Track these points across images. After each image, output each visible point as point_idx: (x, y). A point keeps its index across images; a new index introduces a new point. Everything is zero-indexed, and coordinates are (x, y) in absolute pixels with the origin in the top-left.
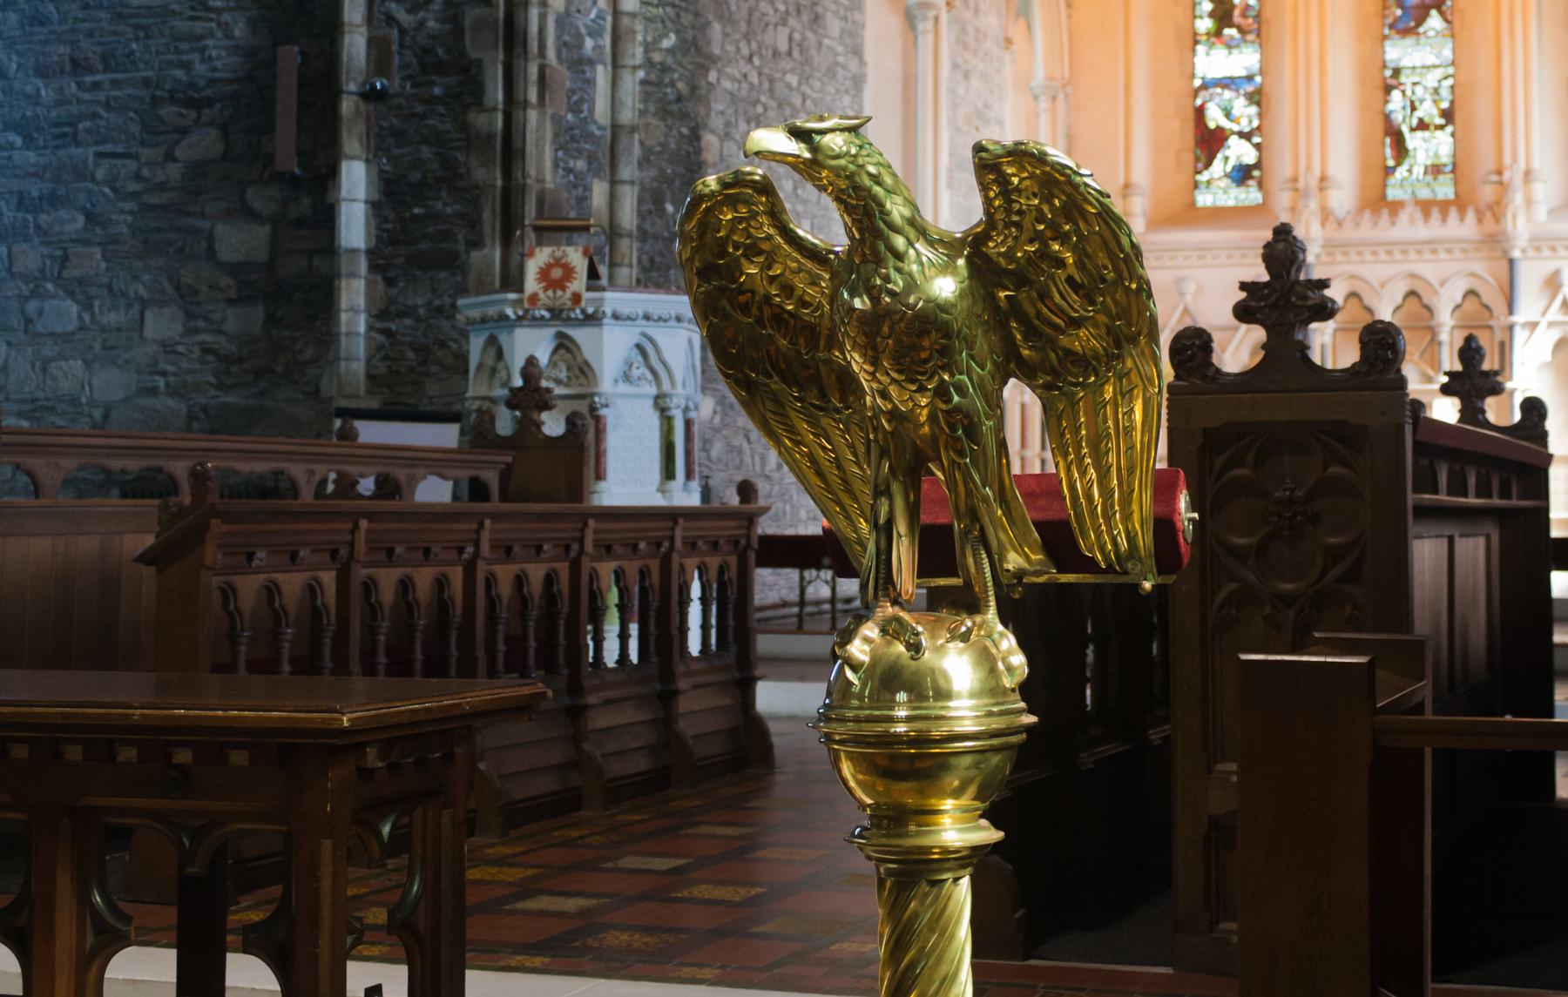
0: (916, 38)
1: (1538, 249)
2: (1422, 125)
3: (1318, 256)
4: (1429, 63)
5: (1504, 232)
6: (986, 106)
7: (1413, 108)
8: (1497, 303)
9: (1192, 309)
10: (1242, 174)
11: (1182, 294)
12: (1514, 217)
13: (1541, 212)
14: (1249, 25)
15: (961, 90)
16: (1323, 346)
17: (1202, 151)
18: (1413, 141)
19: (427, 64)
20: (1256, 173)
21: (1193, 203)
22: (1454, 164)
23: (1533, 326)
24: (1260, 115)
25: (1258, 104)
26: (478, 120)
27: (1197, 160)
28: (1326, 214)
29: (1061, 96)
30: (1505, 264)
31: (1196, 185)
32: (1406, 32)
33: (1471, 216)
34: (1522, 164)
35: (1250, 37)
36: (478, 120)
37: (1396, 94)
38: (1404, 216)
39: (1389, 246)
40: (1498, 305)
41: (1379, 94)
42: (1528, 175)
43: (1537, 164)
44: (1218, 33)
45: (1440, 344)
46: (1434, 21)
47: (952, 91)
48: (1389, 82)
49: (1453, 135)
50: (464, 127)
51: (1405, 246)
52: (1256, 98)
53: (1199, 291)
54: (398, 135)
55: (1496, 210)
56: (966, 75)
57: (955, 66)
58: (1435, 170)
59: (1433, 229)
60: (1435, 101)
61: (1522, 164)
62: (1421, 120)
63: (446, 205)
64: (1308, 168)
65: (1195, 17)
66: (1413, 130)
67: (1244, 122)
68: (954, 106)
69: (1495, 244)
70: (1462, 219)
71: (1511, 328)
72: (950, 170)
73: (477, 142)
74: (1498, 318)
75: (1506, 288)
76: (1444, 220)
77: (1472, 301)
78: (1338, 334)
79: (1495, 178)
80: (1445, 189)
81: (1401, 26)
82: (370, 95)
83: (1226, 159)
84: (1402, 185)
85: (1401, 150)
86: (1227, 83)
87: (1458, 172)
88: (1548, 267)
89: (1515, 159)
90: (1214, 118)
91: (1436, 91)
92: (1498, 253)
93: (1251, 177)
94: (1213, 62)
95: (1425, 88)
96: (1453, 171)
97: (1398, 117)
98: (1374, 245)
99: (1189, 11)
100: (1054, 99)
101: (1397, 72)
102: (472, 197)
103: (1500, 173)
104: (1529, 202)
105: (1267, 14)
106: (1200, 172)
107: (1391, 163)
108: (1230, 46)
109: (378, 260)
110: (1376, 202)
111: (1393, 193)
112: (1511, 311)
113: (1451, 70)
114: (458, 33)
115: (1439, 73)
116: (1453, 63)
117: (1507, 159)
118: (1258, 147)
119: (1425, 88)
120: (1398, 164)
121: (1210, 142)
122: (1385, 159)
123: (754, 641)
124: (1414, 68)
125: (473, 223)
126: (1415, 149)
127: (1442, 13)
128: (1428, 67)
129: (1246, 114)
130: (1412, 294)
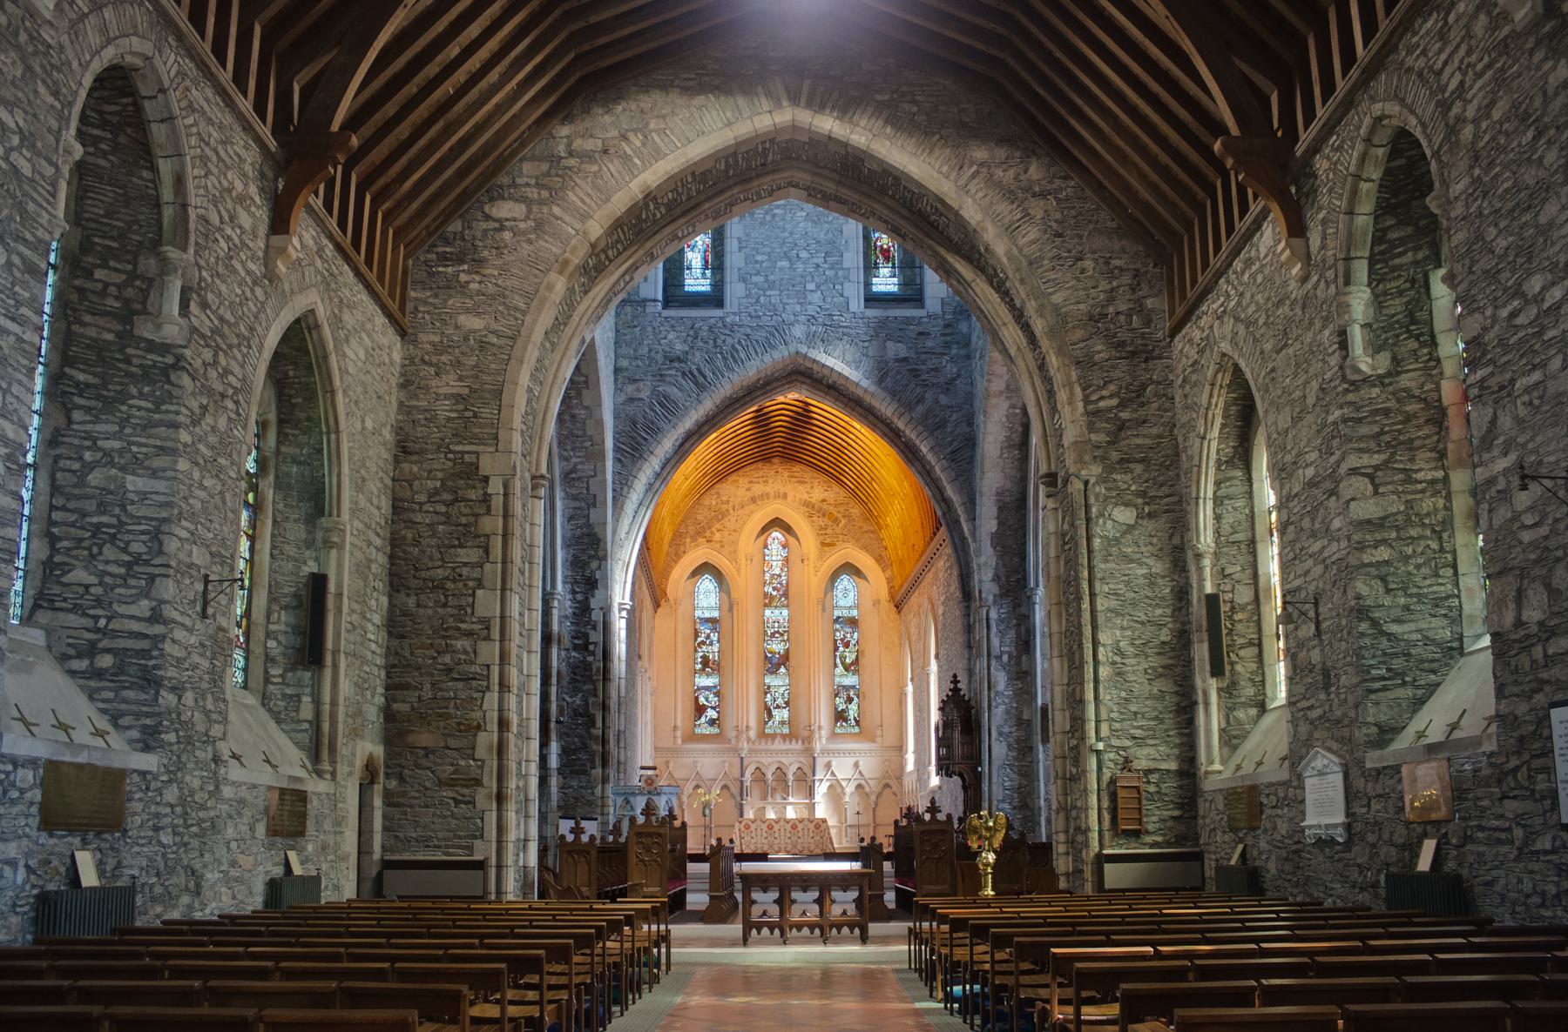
2: (778, 707)
8: (809, 773)
10: (712, 722)
18: (775, 712)
19: (576, 713)
26: (594, 731)
28: (749, 739)
32: (772, 673)
36: (594, 731)
38: (776, 741)
39: (771, 752)
40: (809, 773)
42: (820, 728)
44: (703, 670)
46: (783, 670)
48: (767, 690)
50: (589, 733)
51: (777, 752)
52: (717, 694)
54: (567, 734)
55: (808, 739)
58: (782, 723)
59: (787, 746)
63: (583, 756)
69: (809, 752)
73: (591, 737)
80: (786, 730)
82: (558, 722)
85: (770, 716)
86: (707, 688)
88: (827, 759)
90: (702, 700)
94: (703, 681)
101: (769, 687)
102: (592, 754)
104: (820, 737)
105: (723, 664)
108: (708, 675)
109: (560, 771)
110: (762, 735)
111: (767, 731)
114: (587, 705)
121: (700, 710)
125: (593, 762)
129: (714, 700)
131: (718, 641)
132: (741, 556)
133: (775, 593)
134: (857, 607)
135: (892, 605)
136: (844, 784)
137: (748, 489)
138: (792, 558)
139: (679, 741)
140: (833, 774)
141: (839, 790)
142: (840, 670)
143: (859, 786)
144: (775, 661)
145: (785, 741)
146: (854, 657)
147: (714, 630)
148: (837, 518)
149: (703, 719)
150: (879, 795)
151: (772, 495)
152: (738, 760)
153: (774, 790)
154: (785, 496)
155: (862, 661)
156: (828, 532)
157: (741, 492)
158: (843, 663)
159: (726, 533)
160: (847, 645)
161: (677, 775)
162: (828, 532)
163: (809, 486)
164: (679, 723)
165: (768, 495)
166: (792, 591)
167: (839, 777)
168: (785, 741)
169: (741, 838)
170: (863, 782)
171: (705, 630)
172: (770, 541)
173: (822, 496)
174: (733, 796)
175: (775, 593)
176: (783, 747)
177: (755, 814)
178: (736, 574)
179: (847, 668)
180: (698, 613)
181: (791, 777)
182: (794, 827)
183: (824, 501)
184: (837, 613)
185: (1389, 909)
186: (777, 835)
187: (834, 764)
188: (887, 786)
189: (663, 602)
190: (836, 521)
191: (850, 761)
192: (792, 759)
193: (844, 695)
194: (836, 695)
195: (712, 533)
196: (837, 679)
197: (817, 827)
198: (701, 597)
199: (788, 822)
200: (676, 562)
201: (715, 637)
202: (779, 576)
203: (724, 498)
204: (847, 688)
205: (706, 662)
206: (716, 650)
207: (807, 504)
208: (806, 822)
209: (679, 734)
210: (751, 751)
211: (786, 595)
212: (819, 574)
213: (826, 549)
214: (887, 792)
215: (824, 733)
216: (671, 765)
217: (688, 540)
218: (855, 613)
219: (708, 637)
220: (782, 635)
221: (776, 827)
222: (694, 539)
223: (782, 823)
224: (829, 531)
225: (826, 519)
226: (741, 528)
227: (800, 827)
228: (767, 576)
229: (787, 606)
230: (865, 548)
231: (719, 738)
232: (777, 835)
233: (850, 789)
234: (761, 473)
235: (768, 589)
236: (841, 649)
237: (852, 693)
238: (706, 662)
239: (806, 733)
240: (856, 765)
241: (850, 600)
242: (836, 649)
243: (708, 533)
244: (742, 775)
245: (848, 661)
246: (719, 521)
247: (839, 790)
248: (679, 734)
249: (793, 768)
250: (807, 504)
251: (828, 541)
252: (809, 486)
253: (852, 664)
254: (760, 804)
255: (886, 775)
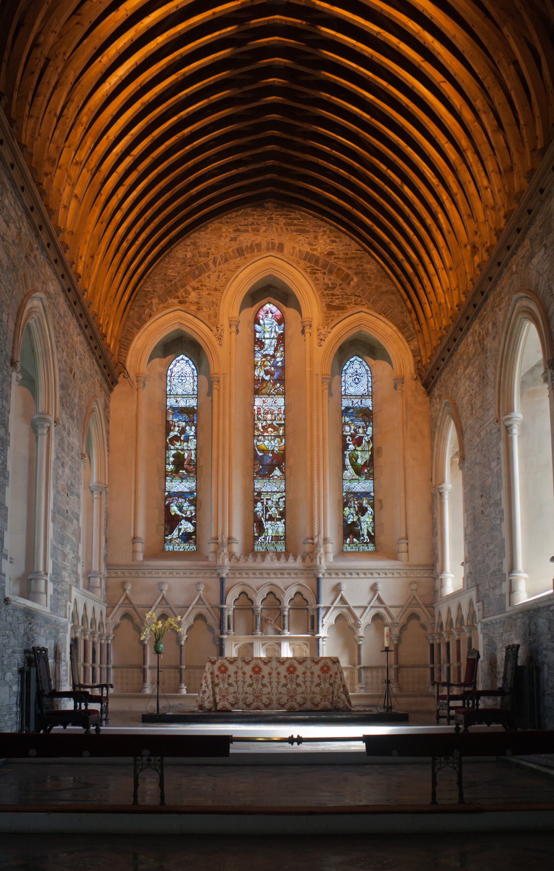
0: (37, 438)
1: (330, 574)
2: (271, 518)
3: (227, 574)
4: (274, 490)
5: (316, 566)
6: (73, 486)
7: (267, 511)
8: (311, 599)
9: (166, 597)
10: (187, 537)
11: (161, 590)
12: (320, 559)
13: (331, 557)
14: (192, 469)
15: (60, 472)
16: (228, 616)
17: (168, 525)
18: (267, 525)
20: (194, 537)
21: (164, 549)
22: (285, 536)
23: (328, 608)
24: (195, 510)
25: (195, 505)
27: (166, 529)
28: (231, 555)
29: (104, 492)
30: (315, 581)
31: (165, 541)
32: (263, 476)
33: (299, 559)
34: (322, 536)
35: (192, 475)
37: (259, 504)
38: (268, 558)
40: (311, 599)
41: (252, 503)
42: (325, 539)
43: (329, 536)
44: (176, 471)
45: (284, 616)
47: (56, 470)
48: (257, 497)
49: (284, 523)
51: (269, 571)
52: (193, 503)
53: (169, 589)
55: (311, 555)
56: (63, 465)
57: (58, 458)
58: (276, 538)
60: (276, 508)
61: (322, 536)
62: (270, 515)
64: (223, 533)
65: (166, 464)
66: (266, 520)
67: (188, 513)
68: (57, 479)
70: (295, 560)
71: (318, 609)
72: (54, 513)
74: (312, 605)
75: (315, 591)
76: (287, 560)
77: (299, 597)
78: (236, 611)
79: (311, 541)
81: (262, 473)
83: (180, 530)
84: (261, 545)
85: (261, 529)
86: (181, 495)
87: (287, 540)
88: (336, 581)
89: (319, 533)
90: (174, 509)
91: (277, 503)
92: (312, 576)
93: (191, 539)
95: (273, 501)
96: (284, 540)
97: (260, 514)
98: (254, 570)
99: (164, 461)
100: (101, 493)
101: (260, 494)
103: (313, 539)
104: (326, 553)
105: (201, 463)
106: (167, 536)
107: (256, 534)
108: (182, 478)
111: (257, 548)
112: (318, 602)
113: (284, 494)
115: (278, 495)
116: (285, 491)
117: (316, 533)
118: (194, 525)
119: (273, 501)
120: (260, 536)
122: (254, 533)
123: (87, 2)
124: (268, 492)
126: (267, 529)
127: (280, 469)
128: (274, 492)
129: (189, 510)
130: (270, 593)
131: (196, 436)
132: (224, 321)
133: (267, 378)
134: (372, 395)
135: (420, 384)
136: (358, 613)
137: (234, 239)
138: (289, 333)
139: (140, 557)
140: (343, 600)
141: (352, 621)
142: (350, 473)
143: (377, 617)
144: (268, 461)
145: (279, 559)
146: (367, 456)
147: (190, 422)
148: (348, 276)
149: (175, 533)
150: (403, 628)
151: (264, 245)
152: (217, 581)
153: (265, 621)
154: (281, 248)
155: (379, 461)
156: (336, 292)
157: (224, 242)
158: (353, 465)
159: (204, 293)
160: (358, 442)
161: (136, 601)
162: (336, 292)
163: (312, 235)
164: (141, 533)
165: (259, 246)
166: (290, 374)
167: (351, 604)
168: (279, 559)
169: (215, 685)
170: (382, 611)
171: (179, 422)
172: (261, 314)
173: (329, 248)
174: (210, 628)
175: (267, 378)
176: (277, 564)
177: (239, 650)
178: (216, 343)
179: (358, 471)
180: (171, 402)
181: (286, 604)
182: (291, 670)
183: (330, 254)
184: (346, 403)
185: (187, 693)
186: (266, 681)
187: (344, 587)
188: (414, 616)
189: (121, 379)
190: (347, 279)
191: (367, 583)
192: (290, 581)
193: (355, 504)
194: (345, 505)
195: (187, 292)
196: (347, 485)
197: (325, 669)
198: (175, 381)
199: (282, 661)
200: (139, 328)
201: (191, 431)
202: (274, 356)
203: (203, 250)
204: (359, 495)
205: (179, 461)
206: (193, 447)
207: (308, 258)
208: (309, 663)
209: (140, 547)
210: (233, 570)
211: (281, 380)
212: (324, 344)
213: (334, 313)
214: (414, 623)
215: (331, 548)
216: (129, 587)
217: (155, 301)
218: (368, 403)
219: (183, 431)
220: (275, 429)
221: (266, 670)
222: (162, 300)
223: (274, 664)
224: (337, 291)
225: (333, 277)
226: (224, 286)
227: (300, 669)
228: (258, 358)
229: (284, 394)
230: (384, 313)
231: (197, 554)
232: (266, 681)
233: (365, 620)
234: (250, 220)
235: (259, 373)
236: (351, 447)
237: (365, 502)
238: (179, 461)
239: (307, 548)
240: (374, 588)
241: (362, 388)
242: (345, 447)
243: (181, 293)
244: (223, 600)
245: (359, 461)
246: (195, 277)
247: (352, 621)
248: (140, 547)
249: (290, 593)
250: (308, 258)
251: (337, 302)
252: (312, 235)
253: (365, 465)
254: (244, 639)
255: (412, 601)
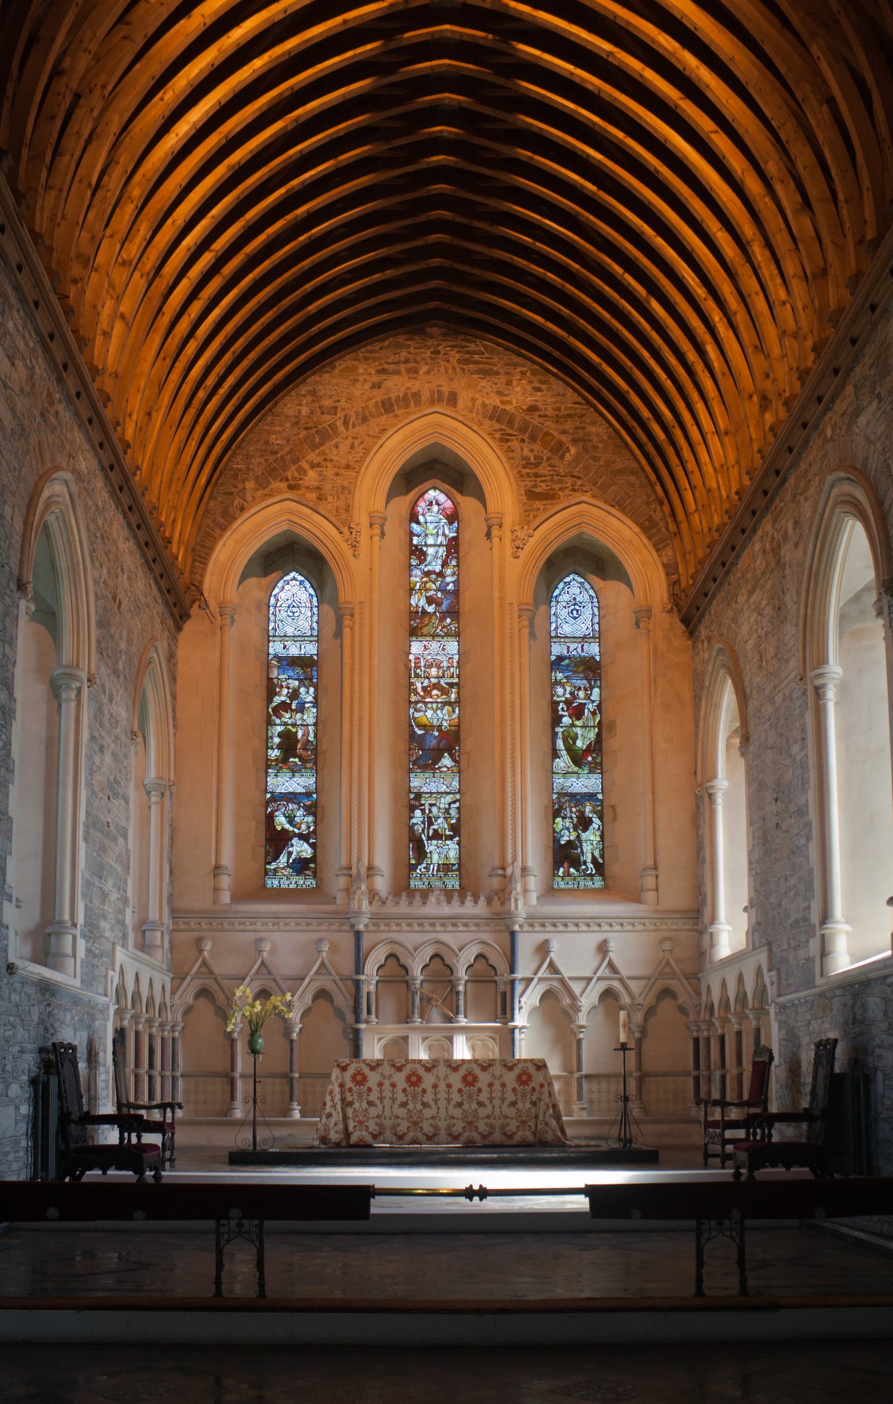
0: (60, 706)
1: (532, 925)
2: (437, 836)
3: (366, 926)
4: (442, 790)
5: (509, 912)
6: (118, 783)
7: (431, 823)
8: (502, 965)
9: (268, 963)
10: (301, 866)
11: (260, 952)
12: (516, 900)
13: (533, 897)
14: (309, 756)
15: (97, 760)
16: (368, 993)
17: (271, 846)
18: (431, 847)
20: (312, 865)
21: (264, 885)
22: (459, 864)
23: (529, 981)
24: (315, 822)
25: (315, 815)
27: (267, 853)
28: (373, 895)
29: (167, 794)
30: (507, 936)
31: (266, 872)
32: (425, 768)
33: (482, 901)
34: (519, 863)
35: (309, 765)
37: (418, 813)
38: (432, 899)
40: (502, 965)
41: (407, 811)
42: (524, 870)
43: (530, 863)
44: (284, 760)
45: (458, 993)
47: (90, 757)
48: (415, 801)
49: (459, 844)
51: (433, 920)
52: (311, 810)
53: (273, 950)
55: (502, 895)
56: (101, 749)
57: (93, 738)
58: (445, 868)
60: (445, 818)
61: (519, 863)
62: (435, 831)
64: (359, 860)
65: (267, 748)
66: (429, 838)
67: (304, 827)
68: (91, 772)
70: (476, 902)
71: (512, 982)
72: (87, 826)
74: (502, 975)
75: (508, 953)
76: (463, 903)
77: (482, 962)
78: (380, 985)
79: (501, 872)
81: (422, 763)
83: (290, 854)
84: (421, 879)
85: (421, 853)
86: (291, 797)
87: (463, 870)
88: (541, 937)
89: (514, 859)
90: (281, 821)
91: (447, 811)
92: (503, 928)
93: (309, 869)
95: (439, 808)
96: (458, 870)
97: (419, 828)
98: (410, 919)
99: (264, 743)
100: (163, 794)
101: (418, 796)
103: (504, 869)
104: (525, 891)
105: (324, 746)
106: (269, 863)
107: (413, 862)
108: (294, 771)
111: (415, 883)
112: (512, 970)
113: (458, 796)
115: (449, 798)
116: (459, 792)
117: (509, 859)
118: (313, 846)
119: (439, 808)
120: (419, 863)
122: (410, 859)
124: (431, 793)
126: (431, 852)
127: (452, 756)
128: (442, 793)
129: (305, 821)
130: (436, 956)
131: (316, 703)
132: (361, 518)
133: (431, 609)
134: (599, 637)
135: (677, 619)
136: (576, 988)
137: (377, 386)
138: (465, 537)
139: (226, 897)
140: (552, 967)
141: (567, 1001)
142: (563, 762)
143: (608, 995)
144: (432, 743)
145: (449, 900)
146: (592, 735)
147: (306, 681)
148: (560, 444)
149: (283, 859)
150: (650, 1012)
151: (425, 396)
152: (350, 937)
153: (427, 1001)
154: (453, 400)
155: (611, 744)
156: (542, 470)
157: (361, 390)
158: (570, 749)
159: (330, 472)
160: (578, 712)
161: (219, 968)
162: (542, 470)
163: (503, 379)
164: (227, 859)
165: (417, 396)
166: (467, 603)
167: (566, 973)
168: (449, 900)
169: (346, 1104)
170: (616, 984)
171: (288, 681)
172: (421, 506)
173: (530, 401)
174: (339, 1013)
175: (431, 609)
176: (447, 910)
177: (385, 1048)
178: (348, 552)
179: (578, 759)
180: (275, 648)
181: (462, 974)
182: (470, 1080)
183: (533, 409)
184: (557, 649)
185: (301, 1117)
186: (428, 1098)
187: (555, 946)
188: (667, 993)
189: (194, 610)
190: (559, 449)
191: (592, 939)
192: (467, 937)
193: (572, 812)
194: (556, 814)
195: (302, 471)
196: (559, 781)
197: (524, 1079)
198: (282, 615)
199: (455, 1066)
200: (224, 529)
201: (307, 695)
202: (441, 574)
203: (327, 403)
204: (578, 799)
205: (289, 743)
206: (311, 720)
207: (497, 415)
208: (497, 1069)
209: (225, 882)
210: (376, 918)
211: (454, 613)
212: (523, 554)
213: (539, 504)
214: (667, 1004)
215: (534, 883)
216: (208, 946)
217: (250, 485)
218: (593, 649)
219: (294, 695)
220: (444, 691)
221: (428, 1080)
222: (262, 483)
223: (442, 1070)
224: (544, 469)
225: (537, 446)
226: (361, 461)
227: (484, 1079)
228: (416, 577)
229: (457, 635)
230: (619, 504)
231: (317, 894)
232: (428, 1098)
233: (588, 999)
234: (404, 354)
235: (418, 601)
236: (566, 720)
237: (588, 809)
238: (289, 743)
239: (495, 883)
240: (603, 948)
241: (583, 625)
242: (556, 720)
243: (291, 473)
244: (359, 968)
245: (579, 743)
246: (314, 447)
247: (567, 1001)
248: (225, 882)
249: (468, 956)
250: (497, 415)
251: (543, 487)
252: (503, 379)
253: (589, 750)
254: (393, 1030)
255: (664, 969)
